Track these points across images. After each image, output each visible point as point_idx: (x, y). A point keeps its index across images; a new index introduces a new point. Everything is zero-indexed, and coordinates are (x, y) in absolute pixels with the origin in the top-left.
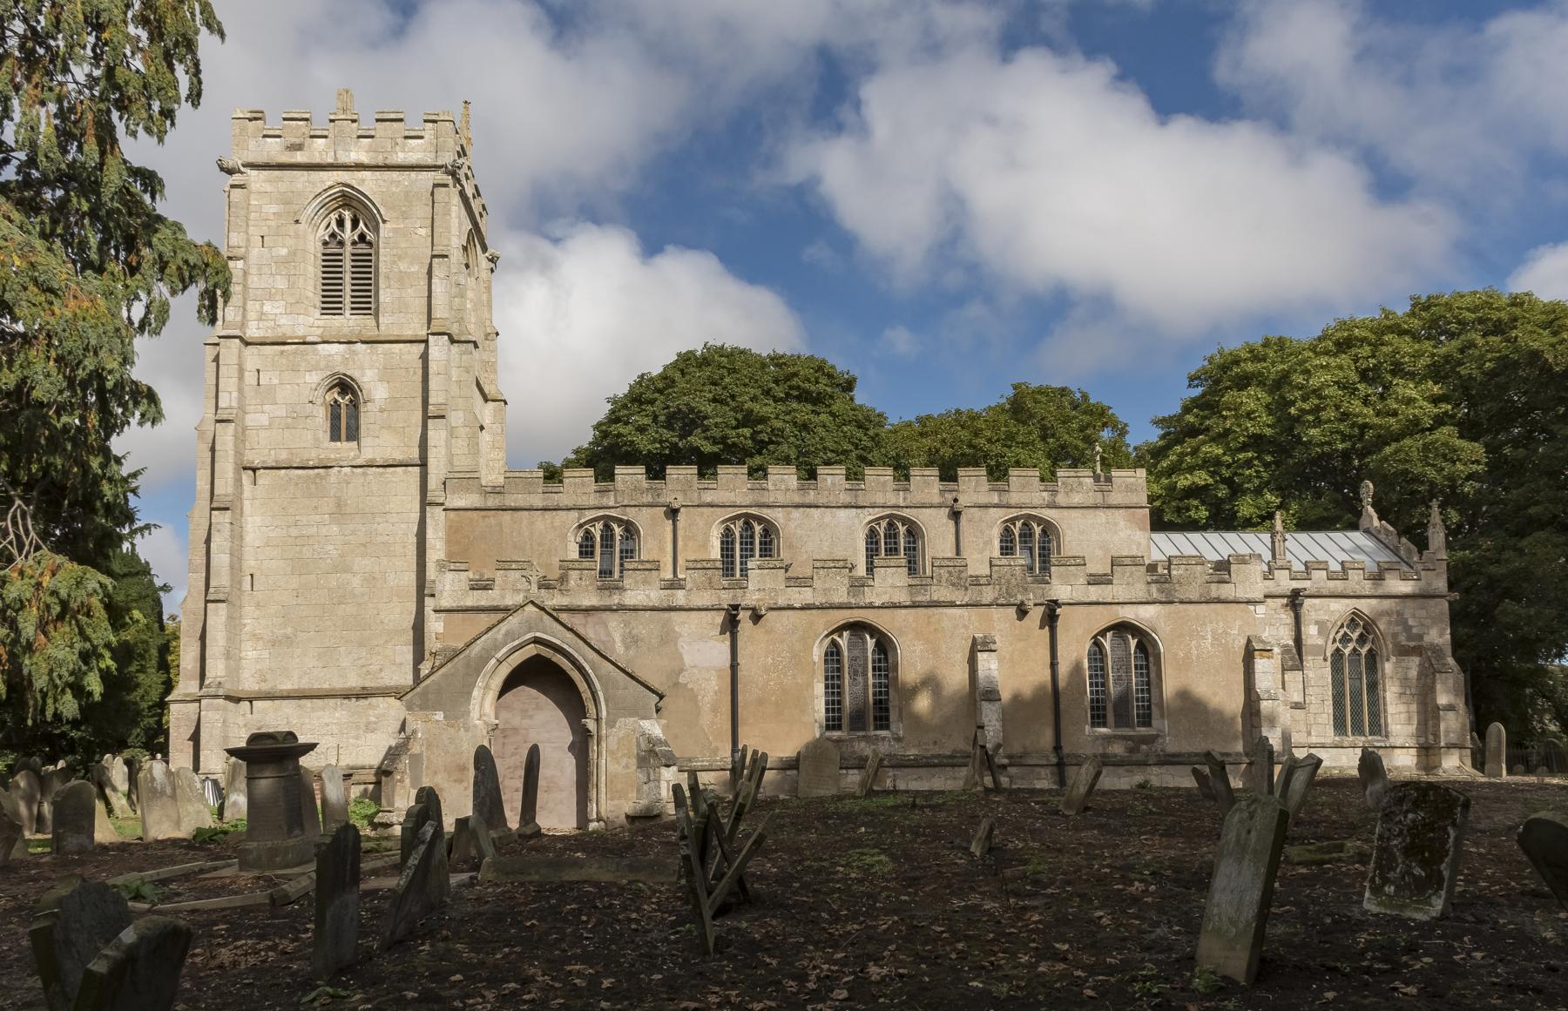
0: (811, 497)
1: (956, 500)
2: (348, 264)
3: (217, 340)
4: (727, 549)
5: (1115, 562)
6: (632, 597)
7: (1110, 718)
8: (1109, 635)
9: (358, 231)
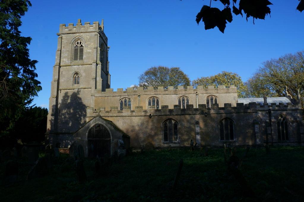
0: (167, 92)
1: (197, 92)
2: (79, 51)
3: (55, 66)
4: (158, 104)
5: (111, 108)
6: (124, 114)
7: (225, 139)
8: (224, 120)
9: (81, 45)
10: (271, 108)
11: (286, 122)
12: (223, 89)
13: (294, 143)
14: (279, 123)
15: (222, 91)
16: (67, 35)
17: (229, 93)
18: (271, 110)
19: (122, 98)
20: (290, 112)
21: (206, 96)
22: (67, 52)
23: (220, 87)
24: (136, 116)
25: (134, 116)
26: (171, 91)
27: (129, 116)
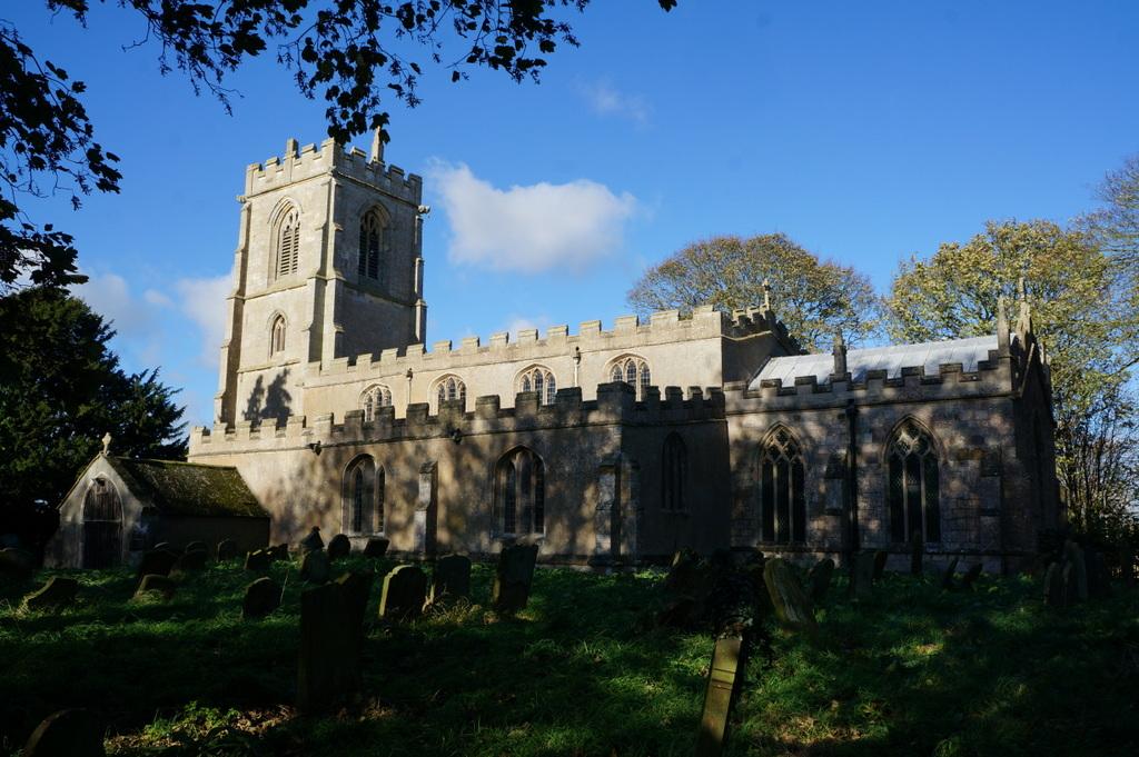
10: (860, 393)
11: (933, 458)
12: (668, 327)
13: (964, 554)
14: (897, 461)
15: (666, 336)
16: (263, 197)
17: (688, 340)
18: (863, 402)
19: (369, 388)
20: (950, 406)
21: (609, 356)
22: (261, 253)
23: (658, 319)
24: (287, 450)
25: (282, 450)
26: (498, 350)
27: (271, 450)
